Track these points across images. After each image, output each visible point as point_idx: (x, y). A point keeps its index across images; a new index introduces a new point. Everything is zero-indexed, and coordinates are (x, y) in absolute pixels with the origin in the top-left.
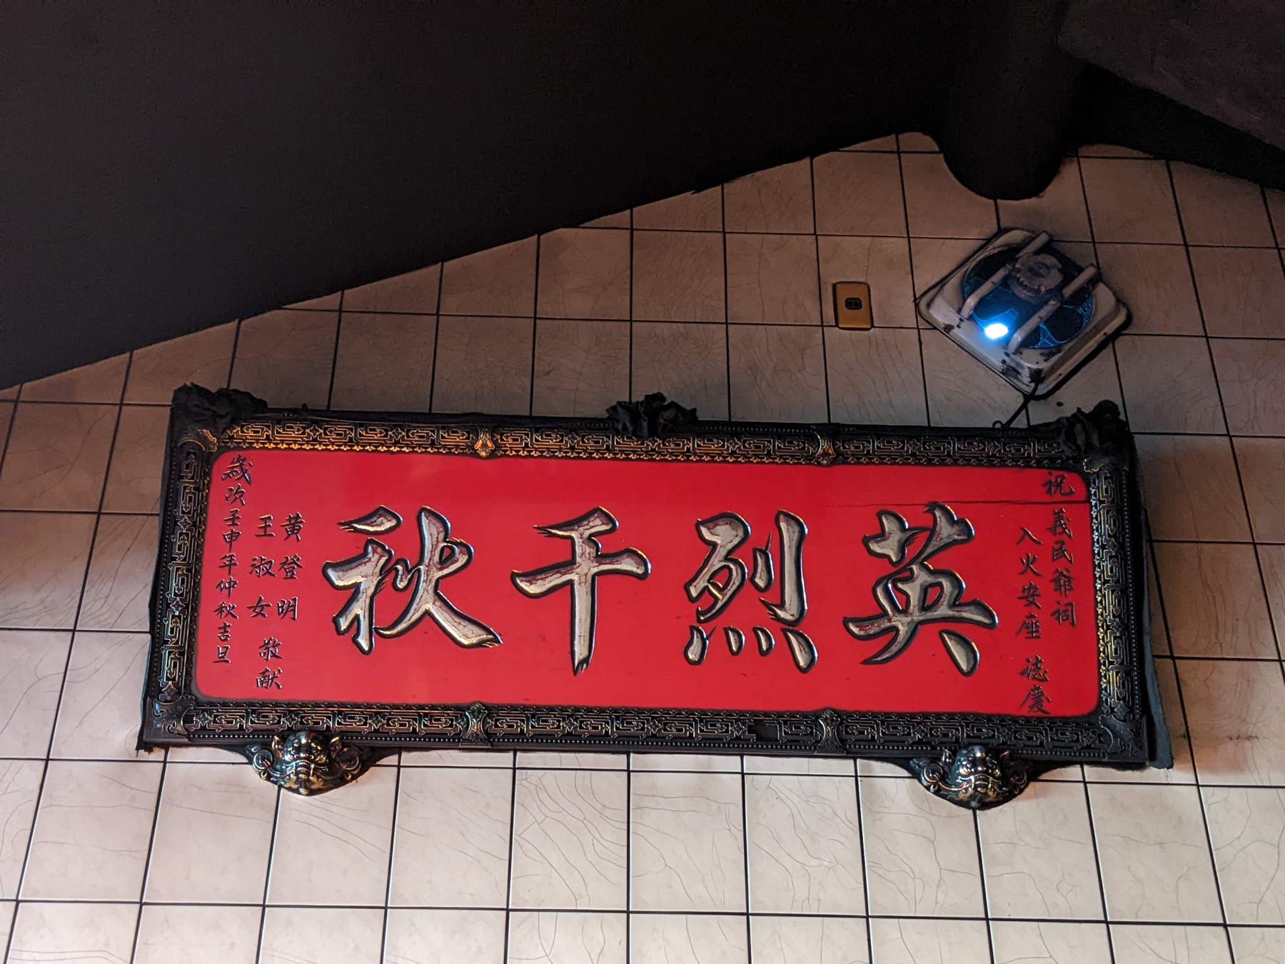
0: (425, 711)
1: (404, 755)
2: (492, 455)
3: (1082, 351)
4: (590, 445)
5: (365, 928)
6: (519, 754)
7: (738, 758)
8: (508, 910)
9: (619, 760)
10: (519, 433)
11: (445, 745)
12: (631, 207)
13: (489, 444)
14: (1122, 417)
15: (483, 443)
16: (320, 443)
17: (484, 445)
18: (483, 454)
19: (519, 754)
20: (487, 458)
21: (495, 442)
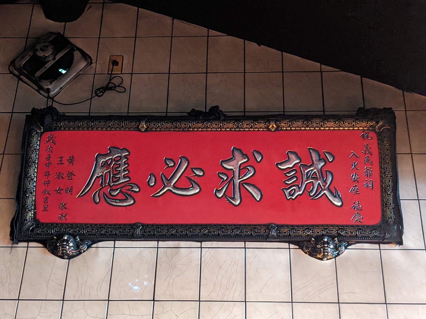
0: (359, 228)
1: (381, 245)
2: (277, 130)
3: (29, 82)
4: (245, 126)
5: (286, 309)
6: (116, 241)
7: (244, 243)
8: (154, 300)
9: (242, 244)
10: (248, 122)
11: (147, 239)
12: (66, 22)
13: (274, 126)
14: (186, 114)
15: (273, 126)
16: (341, 127)
17: (273, 127)
18: (273, 130)
19: (159, 242)
20: (274, 131)
21: (276, 125)
